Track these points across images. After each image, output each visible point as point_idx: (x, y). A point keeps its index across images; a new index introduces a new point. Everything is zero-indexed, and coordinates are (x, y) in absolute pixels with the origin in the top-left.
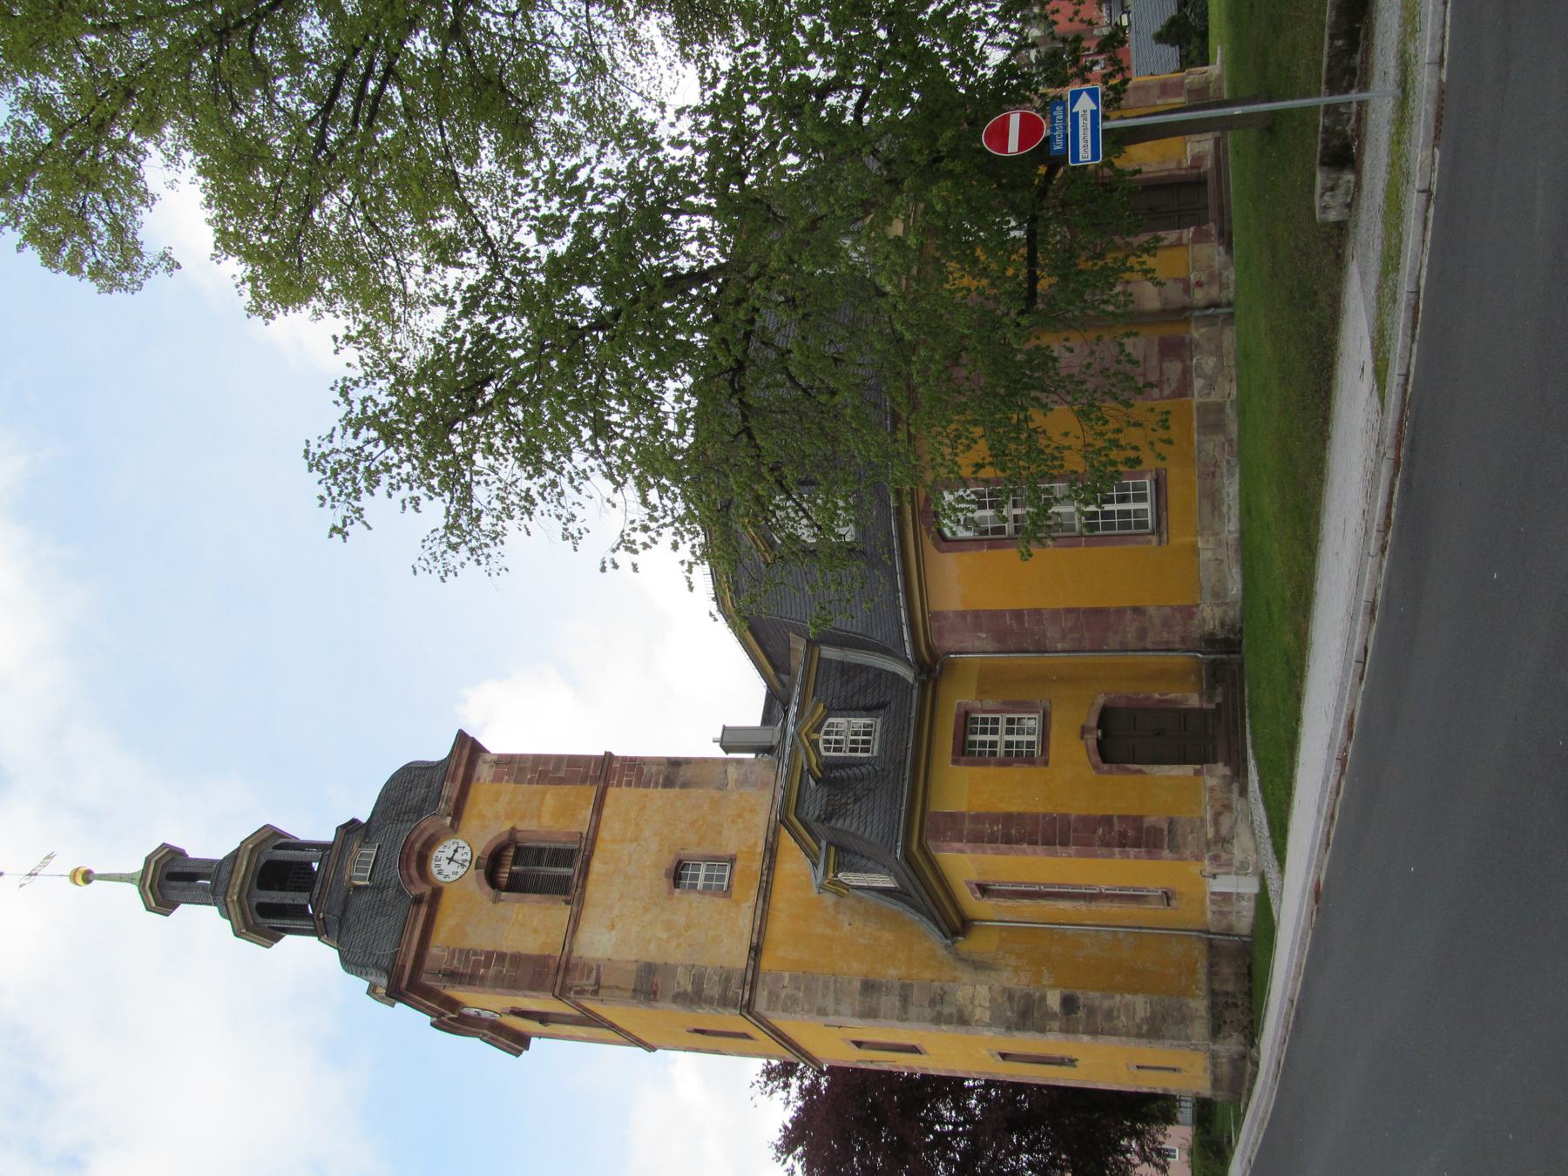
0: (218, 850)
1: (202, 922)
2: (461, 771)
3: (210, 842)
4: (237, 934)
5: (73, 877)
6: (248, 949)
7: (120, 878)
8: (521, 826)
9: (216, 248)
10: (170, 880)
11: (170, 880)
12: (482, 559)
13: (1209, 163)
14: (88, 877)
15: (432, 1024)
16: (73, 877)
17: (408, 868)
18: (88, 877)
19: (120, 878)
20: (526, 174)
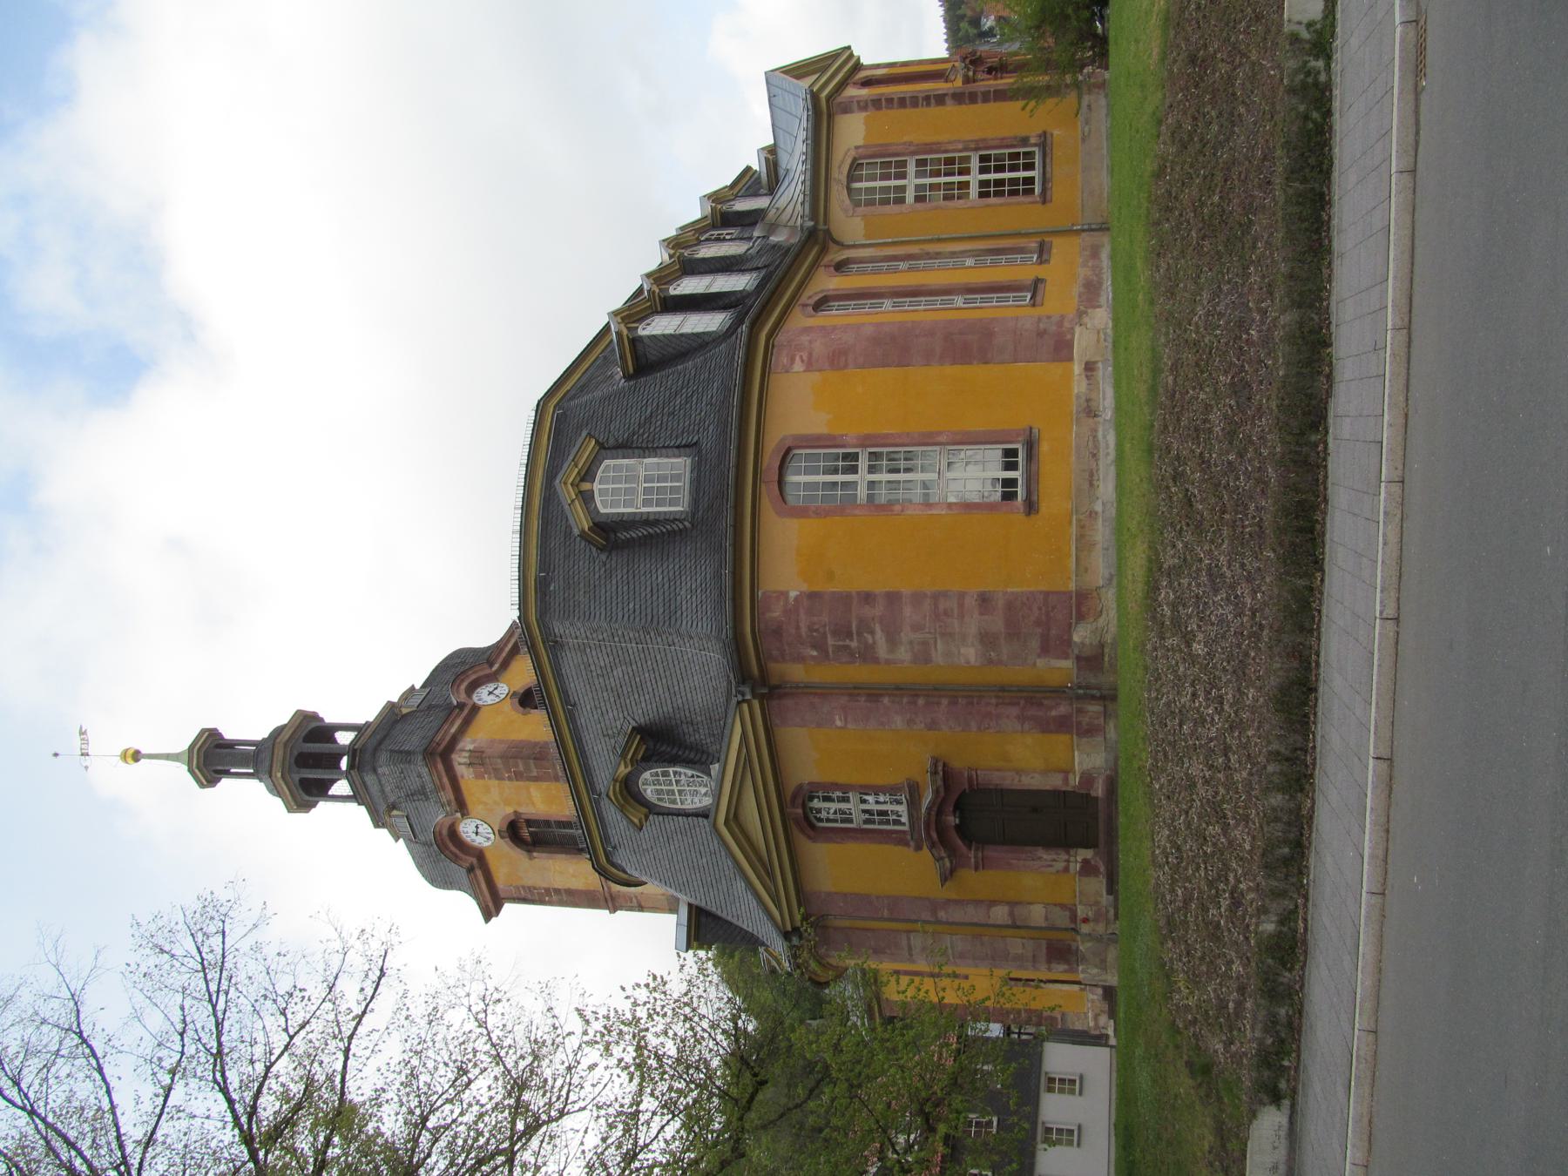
0: (260, 732)
1: (247, 796)
2: (445, 780)
3: (251, 724)
4: (290, 810)
5: (124, 756)
6: (309, 708)
7: (168, 757)
8: (522, 810)
9: (846, 367)
10: (213, 758)
11: (213, 758)
12: (496, 996)
13: (1099, 790)
14: (137, 756)
15: (413, 688)
16: (124, 756)
17: (447, 848)
18: (137, 756)
19: (168, 757)
20: (283, 1085)
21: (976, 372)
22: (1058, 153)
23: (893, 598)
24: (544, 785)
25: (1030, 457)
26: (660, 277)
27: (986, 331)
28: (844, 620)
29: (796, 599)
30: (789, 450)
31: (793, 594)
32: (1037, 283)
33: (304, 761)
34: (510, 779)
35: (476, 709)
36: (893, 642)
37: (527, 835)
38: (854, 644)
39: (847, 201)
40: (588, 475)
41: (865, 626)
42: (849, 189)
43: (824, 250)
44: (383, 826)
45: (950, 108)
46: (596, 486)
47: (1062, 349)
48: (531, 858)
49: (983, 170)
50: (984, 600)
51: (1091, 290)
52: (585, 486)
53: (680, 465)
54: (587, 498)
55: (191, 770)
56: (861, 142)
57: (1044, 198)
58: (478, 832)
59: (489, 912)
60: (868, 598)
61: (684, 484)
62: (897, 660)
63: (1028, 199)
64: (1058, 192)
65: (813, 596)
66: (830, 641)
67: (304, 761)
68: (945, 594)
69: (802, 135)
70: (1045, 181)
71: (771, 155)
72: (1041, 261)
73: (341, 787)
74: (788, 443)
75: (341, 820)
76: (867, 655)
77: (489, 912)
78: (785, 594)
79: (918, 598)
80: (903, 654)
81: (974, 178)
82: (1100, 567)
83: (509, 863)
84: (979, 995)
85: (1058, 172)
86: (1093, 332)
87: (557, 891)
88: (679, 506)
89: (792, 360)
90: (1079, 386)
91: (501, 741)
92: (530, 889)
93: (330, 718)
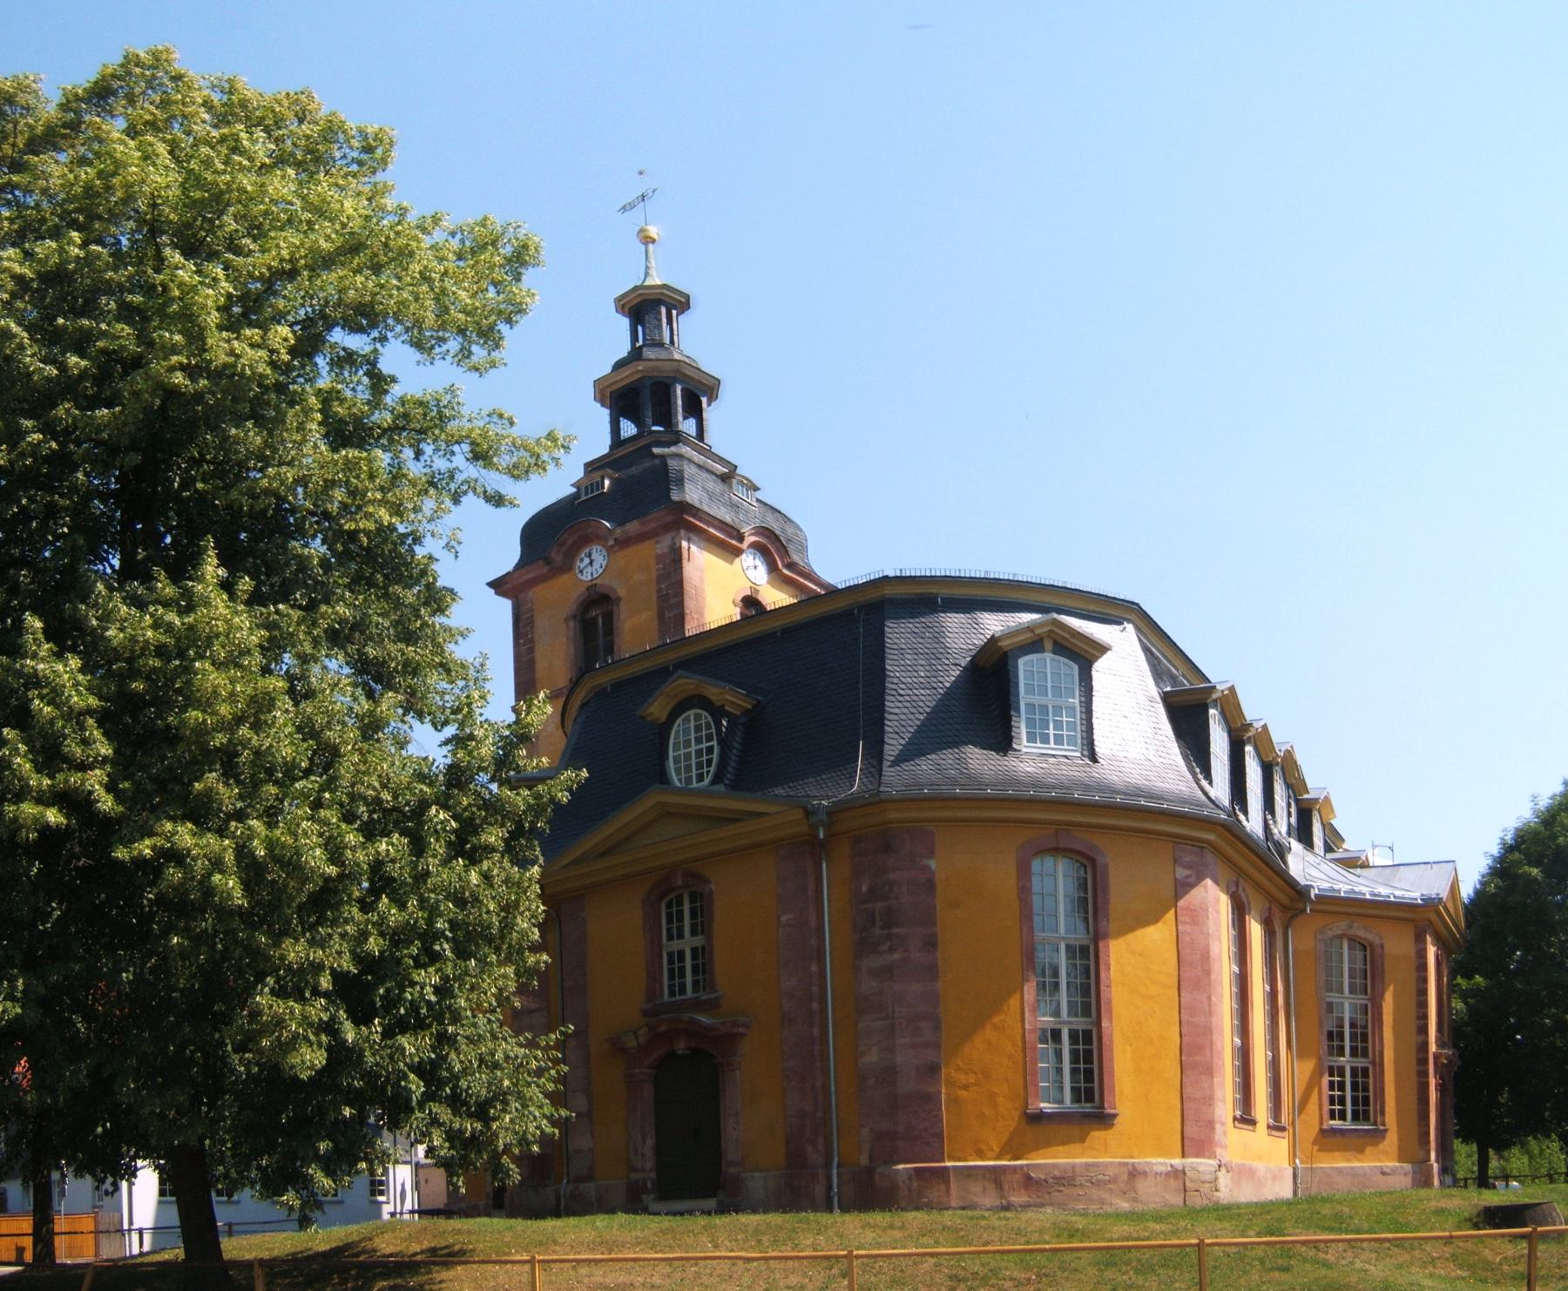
1: (614, 339)
8: (623, 607)
10: (648, 308)
23: (932, 972)
24: (655, 625)
25: (1086, 1116)
26: (1263, 740)
29: (927, 867)
30: (1093, 861)
31: (932, 864)
32: (1253, 1122)
34: (659, 590)
37: (595, 613)
38: (877, 931)
39: (1330, 934)
42: (1341, 937)
43: (1285, 908)
44: (586, 472)
46: (1048, 656)
48: (567, 620)
49: (1354, 1071)
52: (1048, 645)
55: (636, 288)
56: (1386, 951)
58: (593, 565)
59: (498, 586)
60: (931, 944)
63: (1326, 1115)
65: (930, 885)
66: (879, 906)
68: (937, 1028)
69: (1384, 891)
70: (1342, 1132)
72: (1269, 1127)
73: (628, 429)
74: (1100, 860)
77: (498, 586)
78: (931, 853)
83: (558, 598)
84: (1041, 955)
87: (531, 650)
89: (1187, 867)
91: (702, 579)
92: (531, 623)
93: (711, 413)
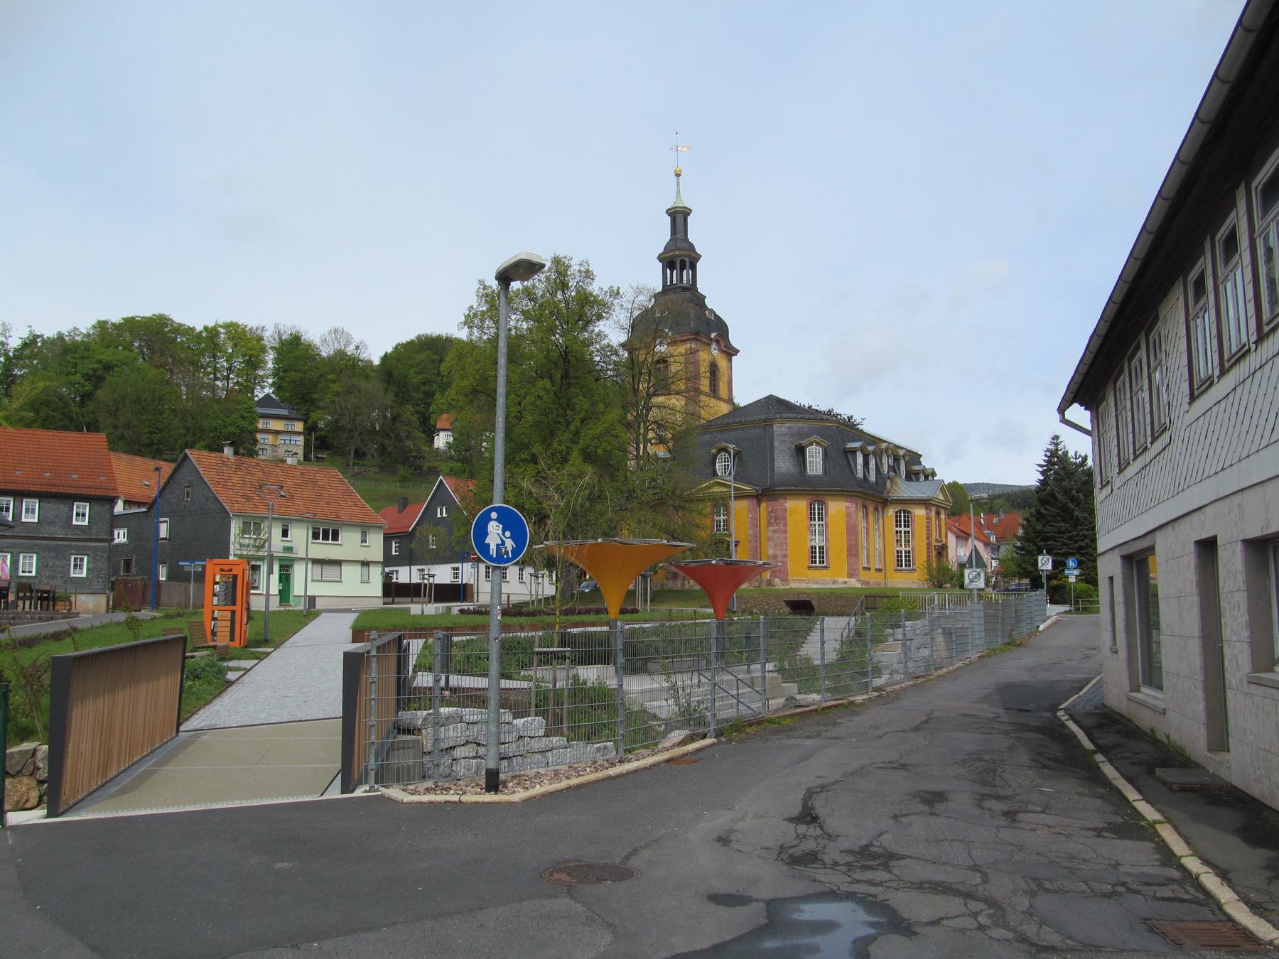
3: (696, 234)
10: (679, 217)
11: (679, 217)
14: (678, 175)
18: (678, 175)
21: (845, 553)
22: (909, 574)
23: (786, 532)
27: (856, 555)
28: (778, 519)
33: (680, 257)
35: (709, 345)
36: (775, 531)
40: (818, 444)
41: (778, 524)
45: (926, 541)
47: (850, 576)
50: (786, 556)
51: (867, 583)
53: (820, 472)
54: (811, 444)
57: (810, 568)
60: (786, 525)
61: (815, 473)
62: (767, 532)
64: (898, 574)
67: (680, 257)
71: (929, 475)
75: (654, 278)
76: (769, 524)
79: (786, 538)
80: (770, 534)
81: (903, 549)
82: (794, 585)
85: (904, 574)
86: (854, 583)
88: (809, 472)
90: (841, 580)
